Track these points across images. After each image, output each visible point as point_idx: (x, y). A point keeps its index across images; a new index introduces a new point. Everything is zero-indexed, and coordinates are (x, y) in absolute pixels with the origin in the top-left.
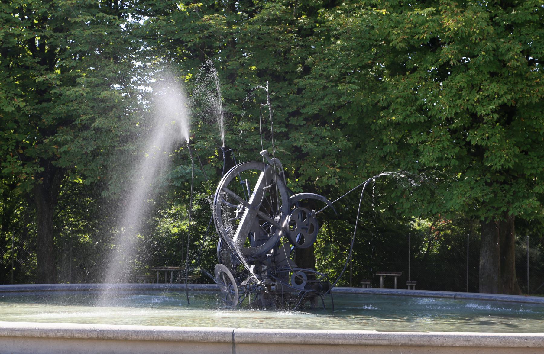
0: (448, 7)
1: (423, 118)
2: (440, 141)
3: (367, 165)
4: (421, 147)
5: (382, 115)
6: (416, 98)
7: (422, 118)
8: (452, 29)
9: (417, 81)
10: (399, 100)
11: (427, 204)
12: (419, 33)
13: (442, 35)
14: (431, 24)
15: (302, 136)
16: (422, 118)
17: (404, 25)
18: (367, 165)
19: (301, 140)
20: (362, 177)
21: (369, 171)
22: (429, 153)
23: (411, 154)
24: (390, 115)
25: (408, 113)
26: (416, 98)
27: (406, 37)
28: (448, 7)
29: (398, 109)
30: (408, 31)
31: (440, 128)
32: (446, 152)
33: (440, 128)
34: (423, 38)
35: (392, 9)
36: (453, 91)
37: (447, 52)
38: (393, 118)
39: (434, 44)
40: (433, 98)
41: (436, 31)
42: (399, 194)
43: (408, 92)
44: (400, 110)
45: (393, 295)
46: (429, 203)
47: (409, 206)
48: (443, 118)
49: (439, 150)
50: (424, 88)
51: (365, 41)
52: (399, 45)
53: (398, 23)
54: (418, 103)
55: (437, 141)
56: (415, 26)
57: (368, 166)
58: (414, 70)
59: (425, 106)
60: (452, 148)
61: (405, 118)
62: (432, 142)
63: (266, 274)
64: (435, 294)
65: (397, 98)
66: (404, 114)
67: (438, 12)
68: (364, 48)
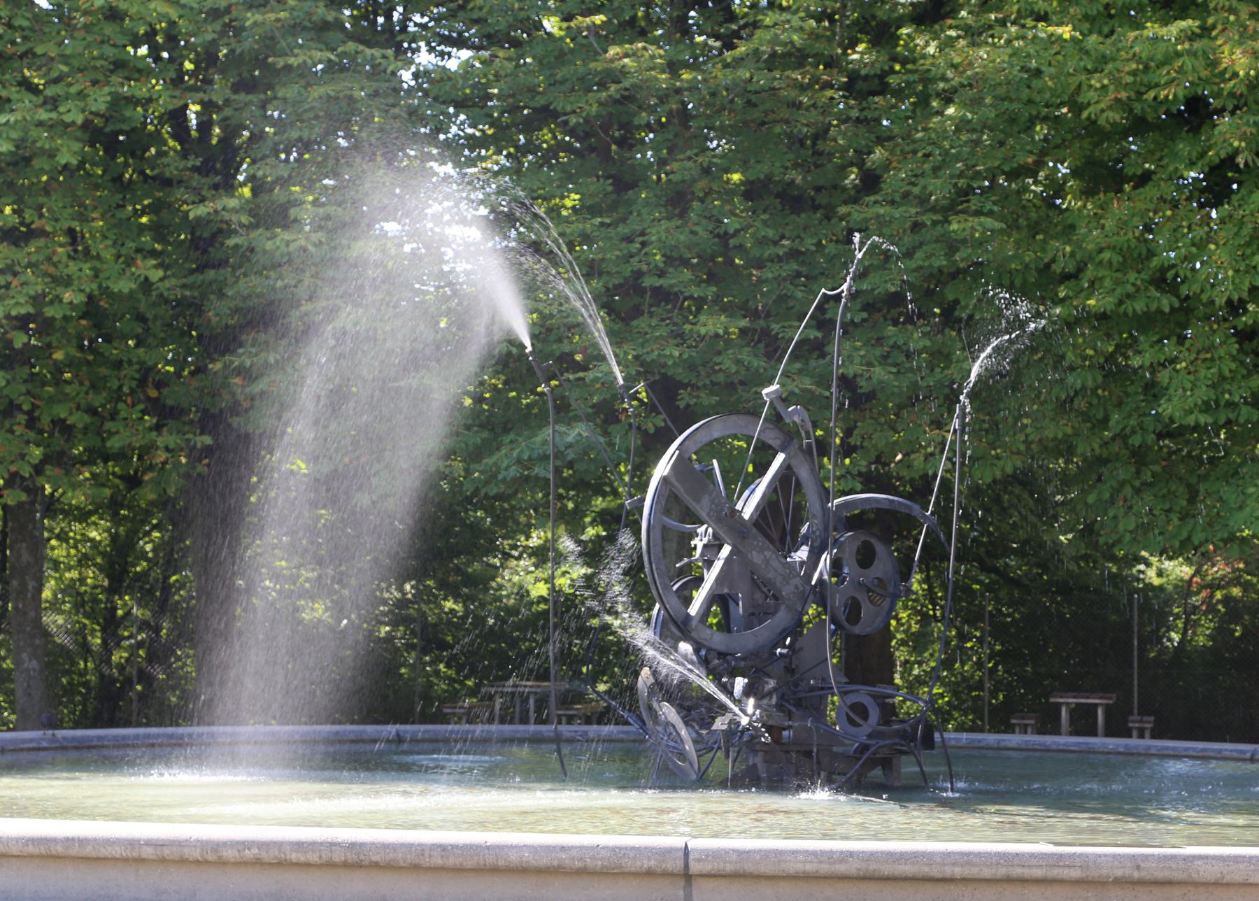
0: (1232, 18)
1: (1166, 303)
2: (1212, 359)
4: (1163, 376)
5: (1062, 295)
6: (1149, 251)
8: (1241, 73)
9: (1152, 206)
10: (1106, 255)
11: (1180, 519)
12: (1157, 85)
13: (1215, 88)
14: (1188, 62)
15: (857, 349)
17: (1118, 64)
19: (857, 360)
20: (1012, 453)
21: (1030, 438)
22: (1184, 390)
23: (1136, 393)
24: (1082, 295)
25: (1130, 289)
26: (1149, 251)
30: (1129, 79)
31: (1211, 328)
34: (1167, 96)
37: (1229, 133)
38: (1092, 302)
40: (1194, 250)
41: (1200, 79)
42: (1107, 495)
44: (1108, 283)
47: (1132, 526)
51: (1018, 109)
52: (1104, 115)
53: (1104, 59)
54: (1155, 262)
55: (1205, 360)
56: (1147, 68)
58: (1144, 179)
61: (1121, 302)
62: (1192, 363)
63: (774, 700)
65: (1100, 251)
66: (1119, 291)
68: (1014, 124)
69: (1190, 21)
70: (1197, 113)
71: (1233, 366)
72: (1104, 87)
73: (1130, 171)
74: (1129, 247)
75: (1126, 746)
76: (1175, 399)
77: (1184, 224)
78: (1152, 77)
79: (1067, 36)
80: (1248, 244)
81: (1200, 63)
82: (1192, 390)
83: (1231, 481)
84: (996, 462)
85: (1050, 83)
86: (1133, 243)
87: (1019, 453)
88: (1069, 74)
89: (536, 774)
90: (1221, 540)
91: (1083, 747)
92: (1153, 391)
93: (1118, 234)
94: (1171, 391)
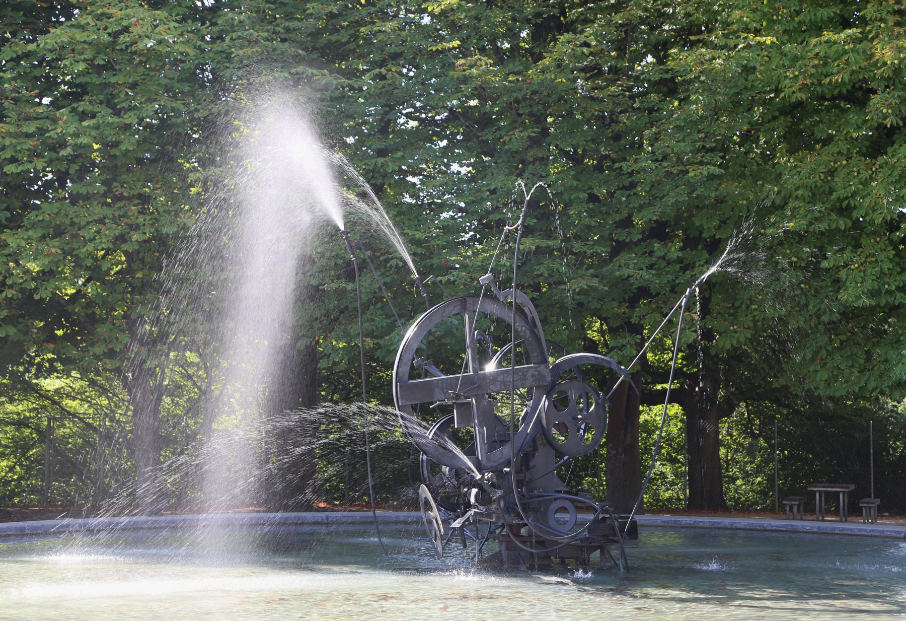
0: (883, 25)
1: (842, 223)
2: (876, 261)
3: (753, 307)
4: (843, 274)
5: (772, 220)
6: (830, 188)
7: (841, 222)
8: (889, 62)
9: (832, 158)
10: (800, 192)
11: (859, 372)
12: (832, 74)
13: (872, 74)
14: (852, 57)
16: (841, 222)
17: (806, 62)
18: (753, 307)
19: (632, 266)
20: (744, 328)
21: (757, 318)
22: (857, 283)
23: (827, 286)
25: (817, 214)
26: (830, 188)
27: (808, 81)
28: (883, 25)
29: (799, 207)
30: (813, 71)
31: (875, 240)
32: (887, 280)
33: (875, 240)
34: (837, 80)
35: (786, 37)
36: (896, 173)
37: (882, 107)
39: (858, 94)
40: (860, 186)
41: (860, 67)
42: (809, 356)
43: (817, 179)
44: (802, 211)
45: (797, 532)
46: (861, 372)
47: (825, 377)
48: (879, 220)
49: (874, 277)
50: (847, 170)
51: (740, 95)
52: (795, 95)
53: (796, 59)
54: (834, 196)
55: (870, 263)
56: (825, 64)
57: (755, 310)
58: (829, 140)
59: (847, 202)
60: (899, 273)
61: (811, 224)
62: (862, 264)
64: (871, 531)
65: (797, 189)
66: (809, 216)
67: (864, 38)
68: (736, 106)
69: (855, 30)
70: (858, 94)
71: (891, 266)
72: (796, 76)
73: (818, 135)
74: (816, 186)
75: (819, 528)
76: (850, 289)
77: (855, 169)
78: (829, 69)
79: (768, 42)
80: (898, 181)
81: (860, 58)
82: (862, 283)
83: (895, 346)
84: (734, 334)
85: (759, 76)
86: (819, 183)
87: (749, 328)
88: (773, 70)
89: (299, 567)
90: (888, 386)
91: (789, 528)
92: (838, 284)
93: (809, 178)
94: (848, 284)
